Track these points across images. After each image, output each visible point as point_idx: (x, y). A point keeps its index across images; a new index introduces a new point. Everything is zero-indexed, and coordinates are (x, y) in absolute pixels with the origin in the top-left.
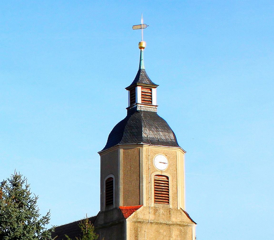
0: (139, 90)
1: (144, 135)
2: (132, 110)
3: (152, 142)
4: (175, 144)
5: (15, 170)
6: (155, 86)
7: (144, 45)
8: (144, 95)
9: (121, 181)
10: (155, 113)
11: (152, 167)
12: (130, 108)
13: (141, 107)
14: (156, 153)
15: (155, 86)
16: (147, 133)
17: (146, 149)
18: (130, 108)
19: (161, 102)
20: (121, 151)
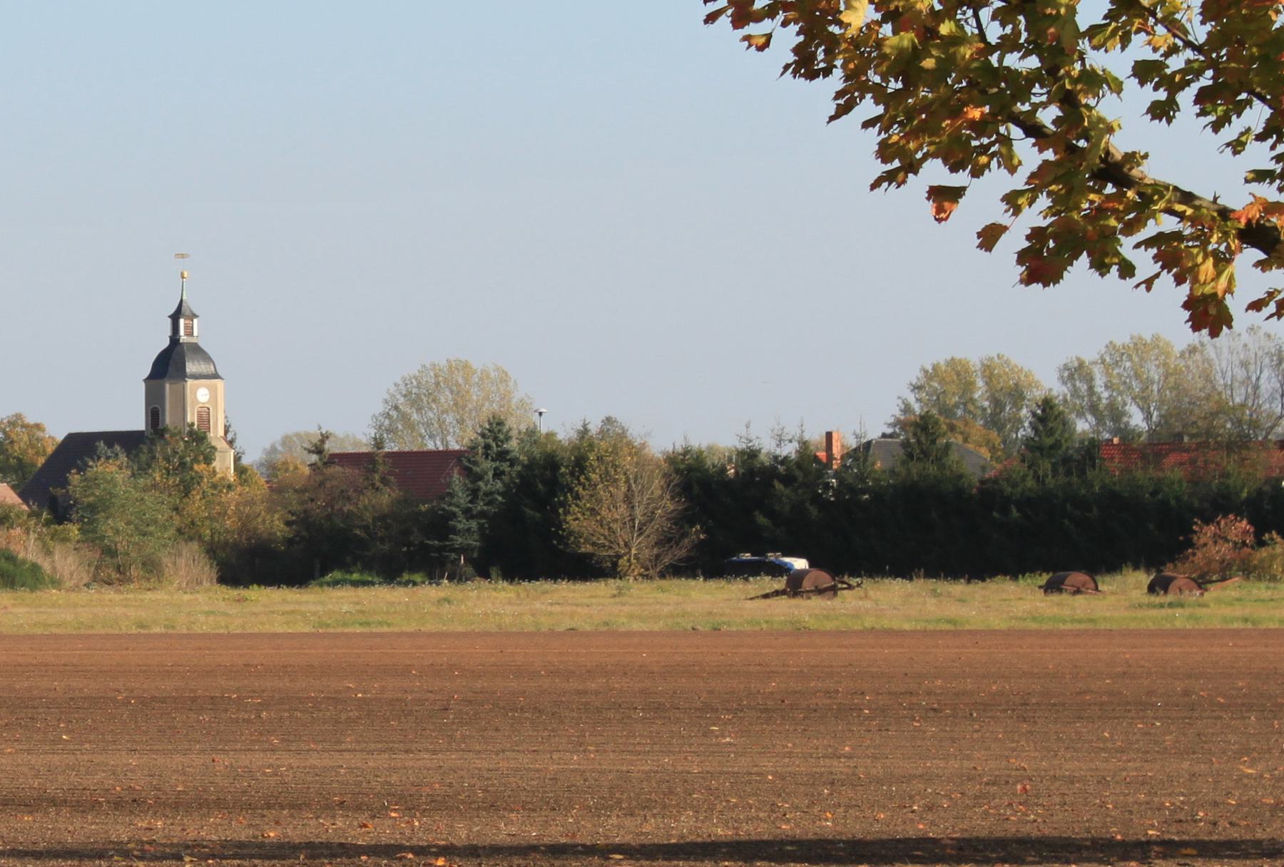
0: (182, 321)
1: (188, 370)
2: (175, 339)
3: (196, 377)
4: (215, 376)
5: (766, 596)
6: (196, 316)
7: (186, 275)
8: (186, 327)
9: (167, 413)
10: (196, 344)
11: (195, 401)
12: (789, 848)
13: (183, 338)
14: (198, 387)
15: (196, 316)
16: (191, 367)
17: (190, 382)
18: (789, 848)
19: (197, 332)
20: (167, 386)
